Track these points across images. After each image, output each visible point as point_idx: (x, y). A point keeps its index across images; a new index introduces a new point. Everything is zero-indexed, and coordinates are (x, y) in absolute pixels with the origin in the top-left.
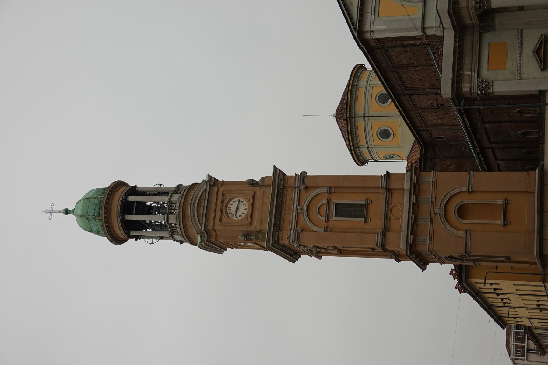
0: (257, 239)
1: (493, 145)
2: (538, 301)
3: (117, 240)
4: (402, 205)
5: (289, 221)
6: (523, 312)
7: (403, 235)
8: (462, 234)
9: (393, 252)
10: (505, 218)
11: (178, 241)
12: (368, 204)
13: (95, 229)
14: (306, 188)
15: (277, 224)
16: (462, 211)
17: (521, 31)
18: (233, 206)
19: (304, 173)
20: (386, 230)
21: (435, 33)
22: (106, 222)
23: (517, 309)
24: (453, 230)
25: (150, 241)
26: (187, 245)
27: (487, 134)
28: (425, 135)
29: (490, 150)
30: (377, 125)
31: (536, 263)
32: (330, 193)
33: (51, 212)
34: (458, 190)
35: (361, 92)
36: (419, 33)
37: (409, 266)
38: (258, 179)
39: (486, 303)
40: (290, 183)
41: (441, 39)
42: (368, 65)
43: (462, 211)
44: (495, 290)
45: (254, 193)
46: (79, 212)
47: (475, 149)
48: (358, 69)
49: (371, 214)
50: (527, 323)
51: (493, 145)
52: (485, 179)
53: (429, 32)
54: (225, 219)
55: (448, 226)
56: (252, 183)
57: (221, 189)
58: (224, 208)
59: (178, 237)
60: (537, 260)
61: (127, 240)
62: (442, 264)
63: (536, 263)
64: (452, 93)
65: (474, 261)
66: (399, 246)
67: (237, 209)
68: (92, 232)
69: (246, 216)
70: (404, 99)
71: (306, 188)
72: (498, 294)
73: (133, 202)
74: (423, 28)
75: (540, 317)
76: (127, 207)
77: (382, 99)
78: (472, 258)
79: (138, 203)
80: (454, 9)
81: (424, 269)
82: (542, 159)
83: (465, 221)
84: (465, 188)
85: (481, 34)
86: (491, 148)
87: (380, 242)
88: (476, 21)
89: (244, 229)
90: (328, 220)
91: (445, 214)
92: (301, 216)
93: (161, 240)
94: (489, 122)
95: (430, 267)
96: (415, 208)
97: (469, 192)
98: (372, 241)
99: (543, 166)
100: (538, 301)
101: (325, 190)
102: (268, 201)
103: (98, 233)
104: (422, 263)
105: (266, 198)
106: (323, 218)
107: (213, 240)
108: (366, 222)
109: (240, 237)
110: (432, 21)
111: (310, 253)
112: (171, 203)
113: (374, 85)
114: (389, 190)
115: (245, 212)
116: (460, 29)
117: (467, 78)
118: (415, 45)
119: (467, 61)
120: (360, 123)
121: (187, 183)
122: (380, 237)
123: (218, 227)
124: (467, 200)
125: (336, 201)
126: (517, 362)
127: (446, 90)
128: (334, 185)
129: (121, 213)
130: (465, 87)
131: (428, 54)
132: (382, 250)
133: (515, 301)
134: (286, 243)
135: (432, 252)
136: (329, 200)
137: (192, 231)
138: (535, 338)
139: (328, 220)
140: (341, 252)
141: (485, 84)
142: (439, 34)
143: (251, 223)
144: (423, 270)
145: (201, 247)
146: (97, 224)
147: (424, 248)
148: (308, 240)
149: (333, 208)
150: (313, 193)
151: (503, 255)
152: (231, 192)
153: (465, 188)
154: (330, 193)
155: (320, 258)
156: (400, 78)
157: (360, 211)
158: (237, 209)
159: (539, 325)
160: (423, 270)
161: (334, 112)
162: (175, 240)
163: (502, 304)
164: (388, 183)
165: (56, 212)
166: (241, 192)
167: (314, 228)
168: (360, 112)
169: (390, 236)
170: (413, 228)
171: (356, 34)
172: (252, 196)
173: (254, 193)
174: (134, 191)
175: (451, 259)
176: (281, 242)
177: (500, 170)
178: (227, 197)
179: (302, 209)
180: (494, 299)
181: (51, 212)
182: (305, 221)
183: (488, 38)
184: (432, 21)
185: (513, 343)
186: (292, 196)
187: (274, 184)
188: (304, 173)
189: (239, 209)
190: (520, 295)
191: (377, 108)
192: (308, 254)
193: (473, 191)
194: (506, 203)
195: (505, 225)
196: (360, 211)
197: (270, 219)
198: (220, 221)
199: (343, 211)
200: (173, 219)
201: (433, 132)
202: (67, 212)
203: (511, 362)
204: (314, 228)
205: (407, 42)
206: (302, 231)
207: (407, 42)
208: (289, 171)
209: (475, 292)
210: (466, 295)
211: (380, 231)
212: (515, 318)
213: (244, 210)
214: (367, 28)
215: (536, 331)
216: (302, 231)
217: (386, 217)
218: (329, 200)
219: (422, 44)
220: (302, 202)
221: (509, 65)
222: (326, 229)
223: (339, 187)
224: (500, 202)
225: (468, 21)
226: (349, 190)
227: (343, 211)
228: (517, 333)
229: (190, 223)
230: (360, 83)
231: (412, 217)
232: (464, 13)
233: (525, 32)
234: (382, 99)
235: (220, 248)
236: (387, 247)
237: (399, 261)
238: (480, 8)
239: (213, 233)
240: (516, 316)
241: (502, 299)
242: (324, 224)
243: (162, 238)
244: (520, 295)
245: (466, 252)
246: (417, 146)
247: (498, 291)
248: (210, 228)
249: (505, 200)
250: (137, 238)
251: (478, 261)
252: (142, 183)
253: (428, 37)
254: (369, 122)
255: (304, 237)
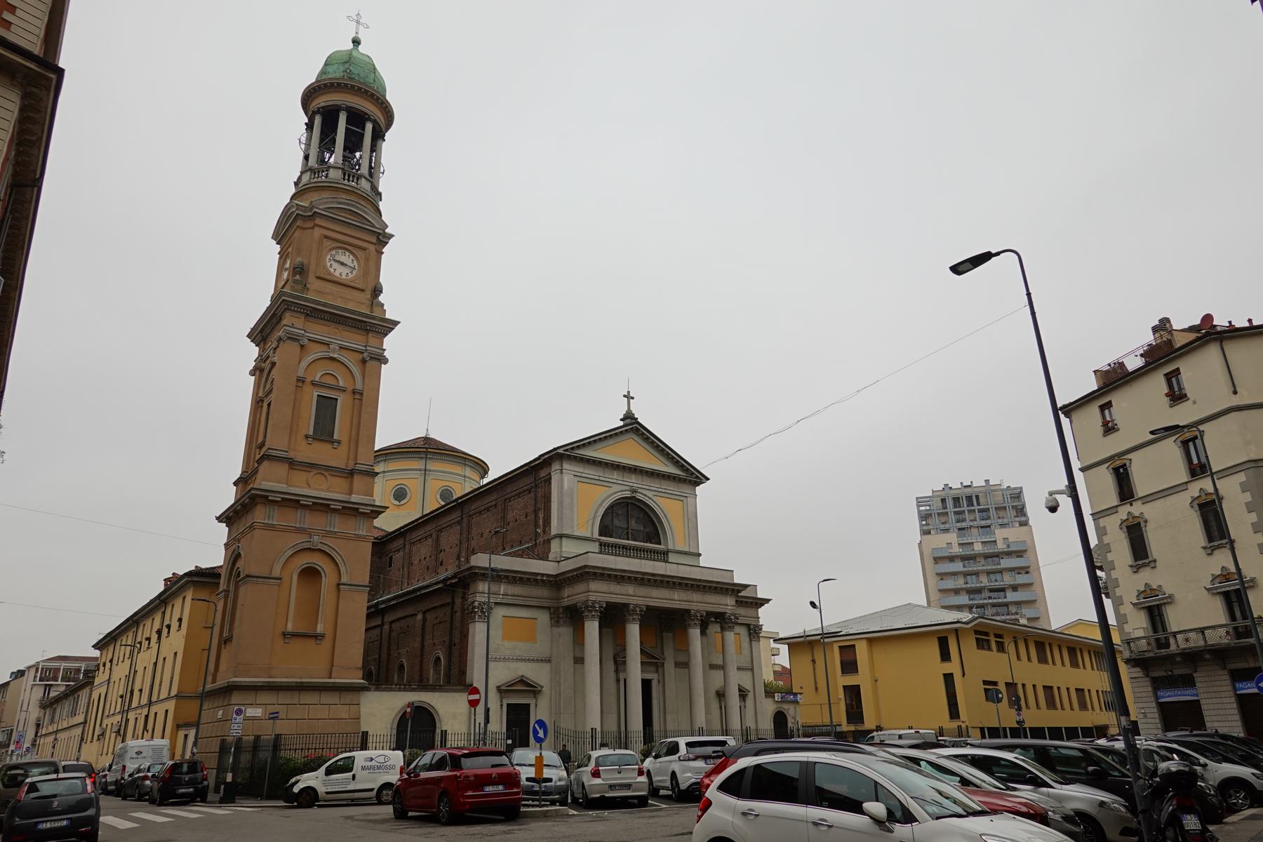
0: (295, 282)
1: (386, 627)
2: (141, 690)
3: (309, 97)
4: (328, 490)
5: (318, 330)
6: (121, 670)
7: (282, 487)
8: (276, 573)
9: (255, 471)
10: (295, 635)
11: (300, 178)
12: (333, 442)
13: (330, 69)
14: (364, 361)
15: (315, 313)
16: (310, 574)
17: (549, 661)
18: (347, 258)
19: (386, 361)
20: (292, 463)
21: (553, 550)
22: (339, 84)
23: (128, 662)
24: (283, 559)
25: (303, 140)
26: (293, 190)
27: (405, 617)
28: (396, 545)
29: (449, 600)
30: (413, 484)
31: (214, 681)
32: (354, 392)
33: (358, 22)
34: (343, 569)
35: (458, 469)
36: (554, 531)
37: (227, 497)
38: (381, 298)
39: (143, 616)
40: (372, 340)
41: (544, 557)
42: (485, 481)
43: (310, 574)
44: (169, 627)
45: (363, 290)
46: (354, 53)
47: (383, 602)
48: (482, 468)
49: (318, 446)
50: (100, 678)
51: (386, 627)
52: (356, 607)
53: (554, 545)
54: (328, 244)
55: (290, 553)
56: (377, 291)
57: (372, 248)
58: (345, 247)
59: (306, 178)
60: (221, 682)
61: (306, 113)
62: (225, 545)
63: (214, 681)
64: (480, 568)
65: (227, 591)
66: (264, 480)
67: (342, 264)
68: (326, 64)
69: (330, 274)
70: (456, 515)
71: (364, 361)
72: (159, 632)
73: (363, 129)
74: (561, 536)
75: (109, 696)
76: (357, 119)
77: (445, 494)
78: (232, 588)
79: (362, 136)
80: (588, 573)
81: (219, 519)
82: (377, 689)
83: (295, 577)
84: (344, 579)
85: (549, 608)
86: (383, 624)
87: (273, 453)
88: (566, 602)
89: (312, 267)
90: (313, 384)
91: (309, 549)
92: (324, 348)
93: (302, 155)
94: (424, 620)
95: (223, 529)
96: (322, 507)
97: (339, 585)
98: (277, 442)
99: (368, 689)
100: (141, 690)
101: (359, 386)
102: (350, 306)
103: (323, 72)
104: (228, 517)
105: (356, 304)
106: (317, 379)
107: (299, 223)
108: (307, 437)
109: (299, 259)
110: (570, 548)
111: (261, 359)
112: (359, 177)
113: (464, 483)
114: (351, 473)
115: (337, 274)
116: (557, 582)
117: (494, 588)
118: (536, 526)
119: (518, 590)
120: (420, 464)
121: (382, 206)
122: (283, 454)
123: (318, 232)
124: (328, 581)
125: (343, 402)
126: (33, 671)
127: (480, 560)
128: (365, 401)
129: (347, 112)
130: (483, 586)
131: (521, 543)
132: (259, 452)
133: (145, 659)
134: (284, 322)
135: (250, 527)
136: (344, 390)
137: (314, 197)
138: (71, 693)
139: (313, 384)
140: (259, 403)
141: (485, 612)
142: (551, 556)
143: (318, 278)
144: (217, 518)
145: (287, 208)
146: (336, 73)
147: (259, 515)
148: (285, 354)
149: (332, 394)
150: (356, 370)
151: (235, 632)
152: (367, 260)
153: (344, 579)
154: (354, 392)
155: (252, 373)
156: (488, 509)
157: (324, 432)
158: (342, 264)
159: (95, 696)
160: (217, 518)
161: (432, 436)
162: (302, 173)
163: (139, 640)
164: (361, 472)
165: (357, 28)
166: (365, 273)
167: (304, 364)
168: (432, 465)
169: (282, 469)
170: (292, 503)
171: (560, 451)
172: (359, 286)
173: (363, 290)
174: (378, 135)
175: (234, 556)
176: (287, 314)
177: (367, 630)
178: (359, 253)
179: (334, 351)
180: (149, 628)
181: (358, 22)
182: (316, 352)
183: (543, 618)
184: (570, 548)
185: (63, 665)
186: (355, 340)
187: (374, 318)
188: (386, 361)
189: (342, 266)
190: (155, 664)
191: (435, 486)
192: (260, 355)
193: (339, 590)
194: (317, 637)
195: (284, 634)
196: (324, 432)
197: (325, 305)
198: (326, 237)
199: (326, 407)
200: (335, 175)
201: (401, 554)
202: (356, 42)
203: (33, 663)
204: (304, 364)
205: (541, 516)
206: (302, 346)
207: (541, 516)
208: (391, 343)
209: (167, 598)
210: (162, 588)
211: (291, 454)
212: (111, 661)
213: (340, 272)
214: (566, 466)
215: (84, 694)
216: (302, 346)
217: (312, 466)
218: (344, 390)
219: (537, 534)
220: (344, 352)
221: (506, 644)
222: (301, 380)
223: (361, 405)
224: (320, 628)
225: (567, 592)
226: (355, 420)
227: (326, 407)
228: (78, 671)
229: (326, 194)
230: (468, 469)
231: (309, 502)
232: (580, 587)
233: (547, 666)
234: (445, 494)
235: (282, 235)
236: (266, 463)
237: (235, 484)
238: (587, 607)
239: (310, 224)
240: (115, 662)
241: (149, 639)
242: (309, 380)
243: (306, 158)
244: (155, 664)
245: (247, 576)
246: (382, 534)
247: (165, 630)
248: (318, 221)
249: (323, 636)
250: (310, 126)
251: (226, 597)
252: (389, 146)
253: (548, 541)
254: (417, 474)
255: (290, 349)
